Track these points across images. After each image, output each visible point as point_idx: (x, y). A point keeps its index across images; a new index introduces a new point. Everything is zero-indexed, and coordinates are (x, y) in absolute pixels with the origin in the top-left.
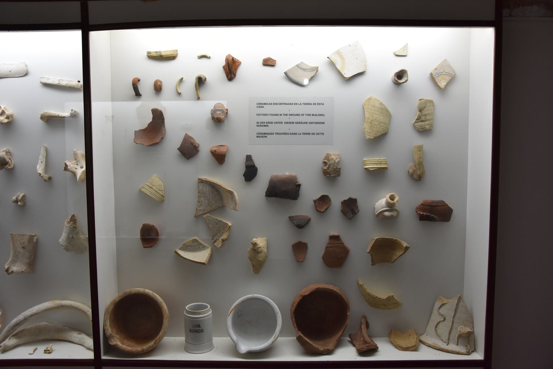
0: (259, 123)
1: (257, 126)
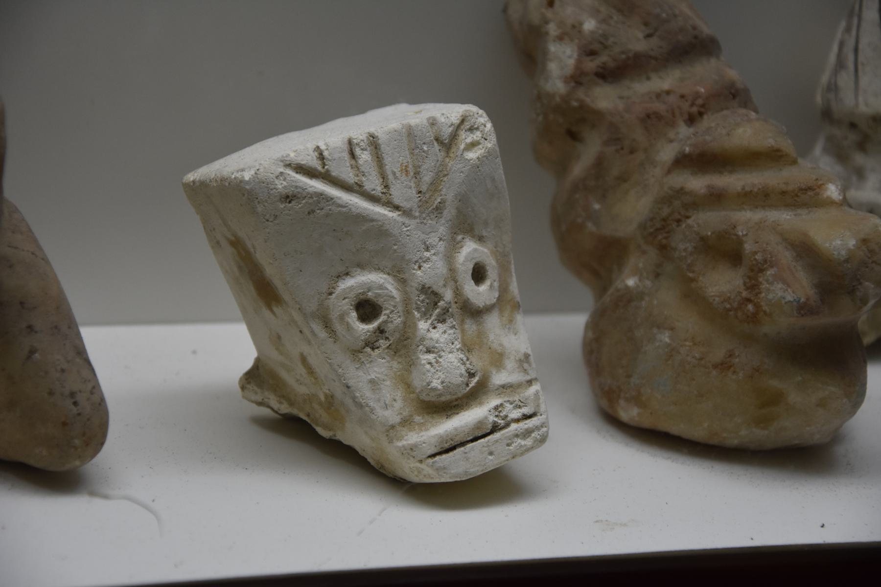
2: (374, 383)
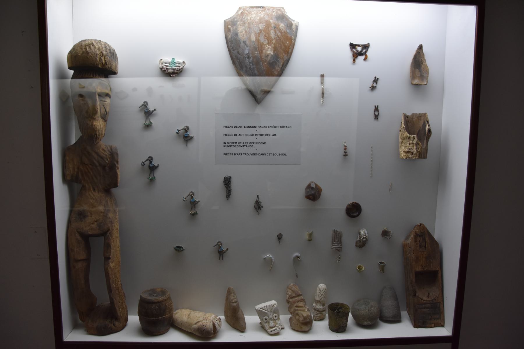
0: (226, 143)
1: (224, 146)
2: (266, 326)
